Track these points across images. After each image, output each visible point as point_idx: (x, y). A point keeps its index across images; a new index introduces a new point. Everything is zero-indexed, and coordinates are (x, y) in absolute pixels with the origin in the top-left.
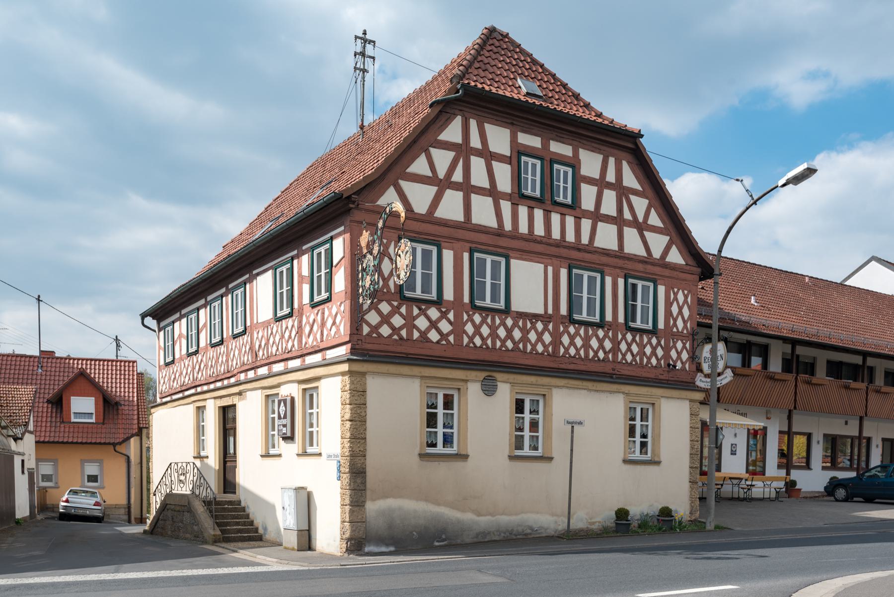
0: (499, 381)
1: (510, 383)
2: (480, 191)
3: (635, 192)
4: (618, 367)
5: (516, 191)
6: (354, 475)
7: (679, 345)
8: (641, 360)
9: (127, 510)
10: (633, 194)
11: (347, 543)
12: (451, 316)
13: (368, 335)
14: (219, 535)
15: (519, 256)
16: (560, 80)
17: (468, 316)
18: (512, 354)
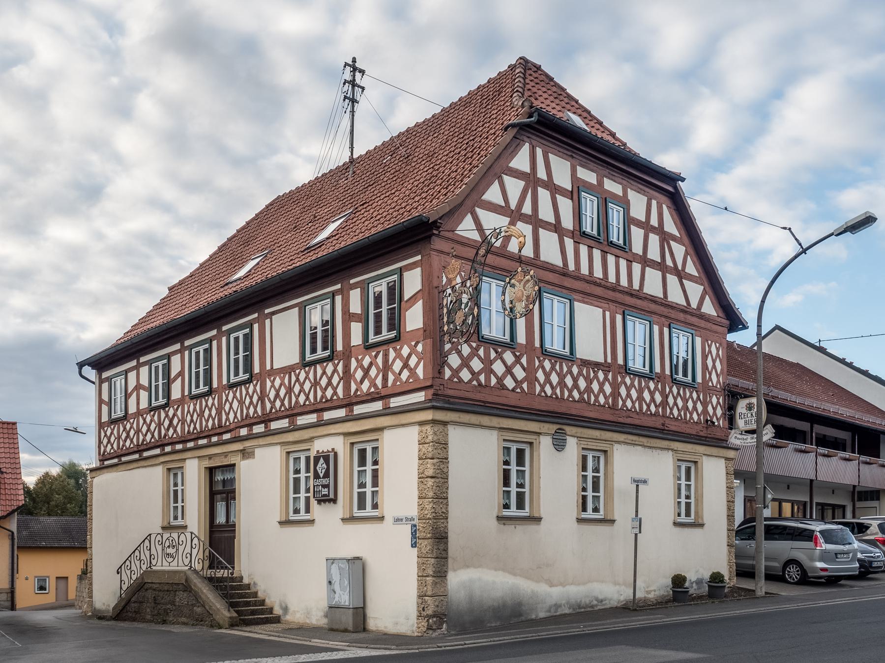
0: (568, 435)
1: (578, 437)
2: (546, 225)
3: (674, 238)
4: (667, 421)
5: (578, 228)
6: (437, 540)
7: (714, 400)
8: (685, 414)
9: (10, 595)
10: (672, 240)
11: (428, 621)
12: (524, 360)
13: (450, 379)
14: (236, 617)
15: (581, 298)
16: (595, 118)
17: (539, 361)
18: (578, 405)
